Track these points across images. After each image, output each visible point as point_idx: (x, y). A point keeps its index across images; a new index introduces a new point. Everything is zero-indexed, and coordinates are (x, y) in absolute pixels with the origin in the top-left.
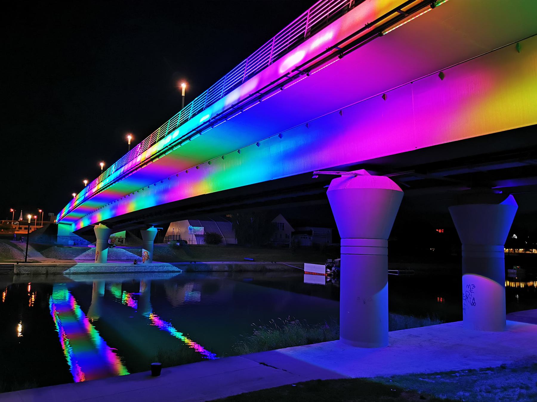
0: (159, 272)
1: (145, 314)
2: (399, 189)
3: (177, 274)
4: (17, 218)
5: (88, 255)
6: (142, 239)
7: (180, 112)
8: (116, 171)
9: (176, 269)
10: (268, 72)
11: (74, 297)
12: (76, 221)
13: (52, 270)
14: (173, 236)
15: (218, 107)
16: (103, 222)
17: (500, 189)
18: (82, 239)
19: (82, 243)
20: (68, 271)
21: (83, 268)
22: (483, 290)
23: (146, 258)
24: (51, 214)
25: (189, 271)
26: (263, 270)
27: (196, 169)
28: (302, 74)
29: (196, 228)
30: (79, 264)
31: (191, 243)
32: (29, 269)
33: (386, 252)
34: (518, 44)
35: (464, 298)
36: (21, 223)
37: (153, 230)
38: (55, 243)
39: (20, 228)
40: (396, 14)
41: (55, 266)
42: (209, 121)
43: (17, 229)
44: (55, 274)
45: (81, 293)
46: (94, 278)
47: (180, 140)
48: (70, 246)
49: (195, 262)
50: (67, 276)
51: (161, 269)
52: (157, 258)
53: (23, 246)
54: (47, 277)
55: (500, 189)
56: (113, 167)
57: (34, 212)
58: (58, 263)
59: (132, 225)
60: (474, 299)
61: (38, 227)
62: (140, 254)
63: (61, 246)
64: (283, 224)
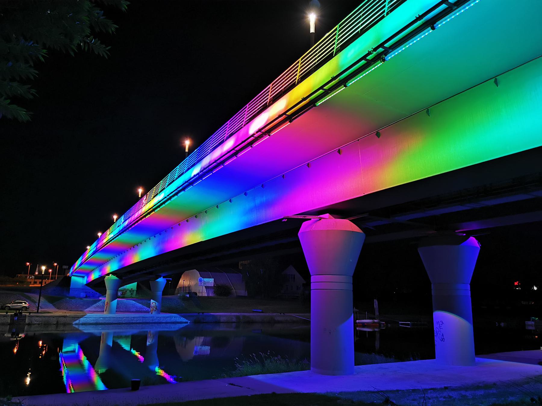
0: (166, 323)
1: (151, 367)
2: (362, 232)
3: (185, 325)
4: (32, 273)
5: (98, 307)
6: (150, 289)
7: (178, 167)
8: (124, 221)
9: (183, 320)
10: (242, 132)
11: (83, 351)
12: (88, 274)
13: (62, 320)
14: (184, 288)
15: (206, 161)
16: (113, 273)
17: (464, 232)
18: (94, 291)
19: (93, 296)
20: (77, 322)
21: (92, 319)
22: (454, 326)
23: (154, 309)
24: (65, 267)
25: (197, 322)
26: (272, 322)
27: (192, 219)
28: (265, 135)
29: (206, 280)
30: (88, 315)
31: (200, 295)
32: (41, 319)
33: (350, 287)
34: (428, 110)
35: (435, 334)
36: (37, 277)
37: (161, 281)
38: (67, 295)
39: (35, 283)
40: (321, 91)
41: (65, 317)
42: (198, 174)
43: (32, 283)
44: (65, 324)
45: (90, 345)
46: (103, 329)
47: (176, 191)
48: (81, 298)
49: (203, 313)
50: (76, 326)
51: (168, 320)
52: (163, 309)
53: (36, 297)
54: (57, 327)
55: (464, 232)
56: (123, 217)
57: (49, 266)
58: (68, 313)
59: (138, 274)
60: (443, 335)
61: (52, 281)
62: (149, 306)
63: (74, 297)
64: (294, 275)
